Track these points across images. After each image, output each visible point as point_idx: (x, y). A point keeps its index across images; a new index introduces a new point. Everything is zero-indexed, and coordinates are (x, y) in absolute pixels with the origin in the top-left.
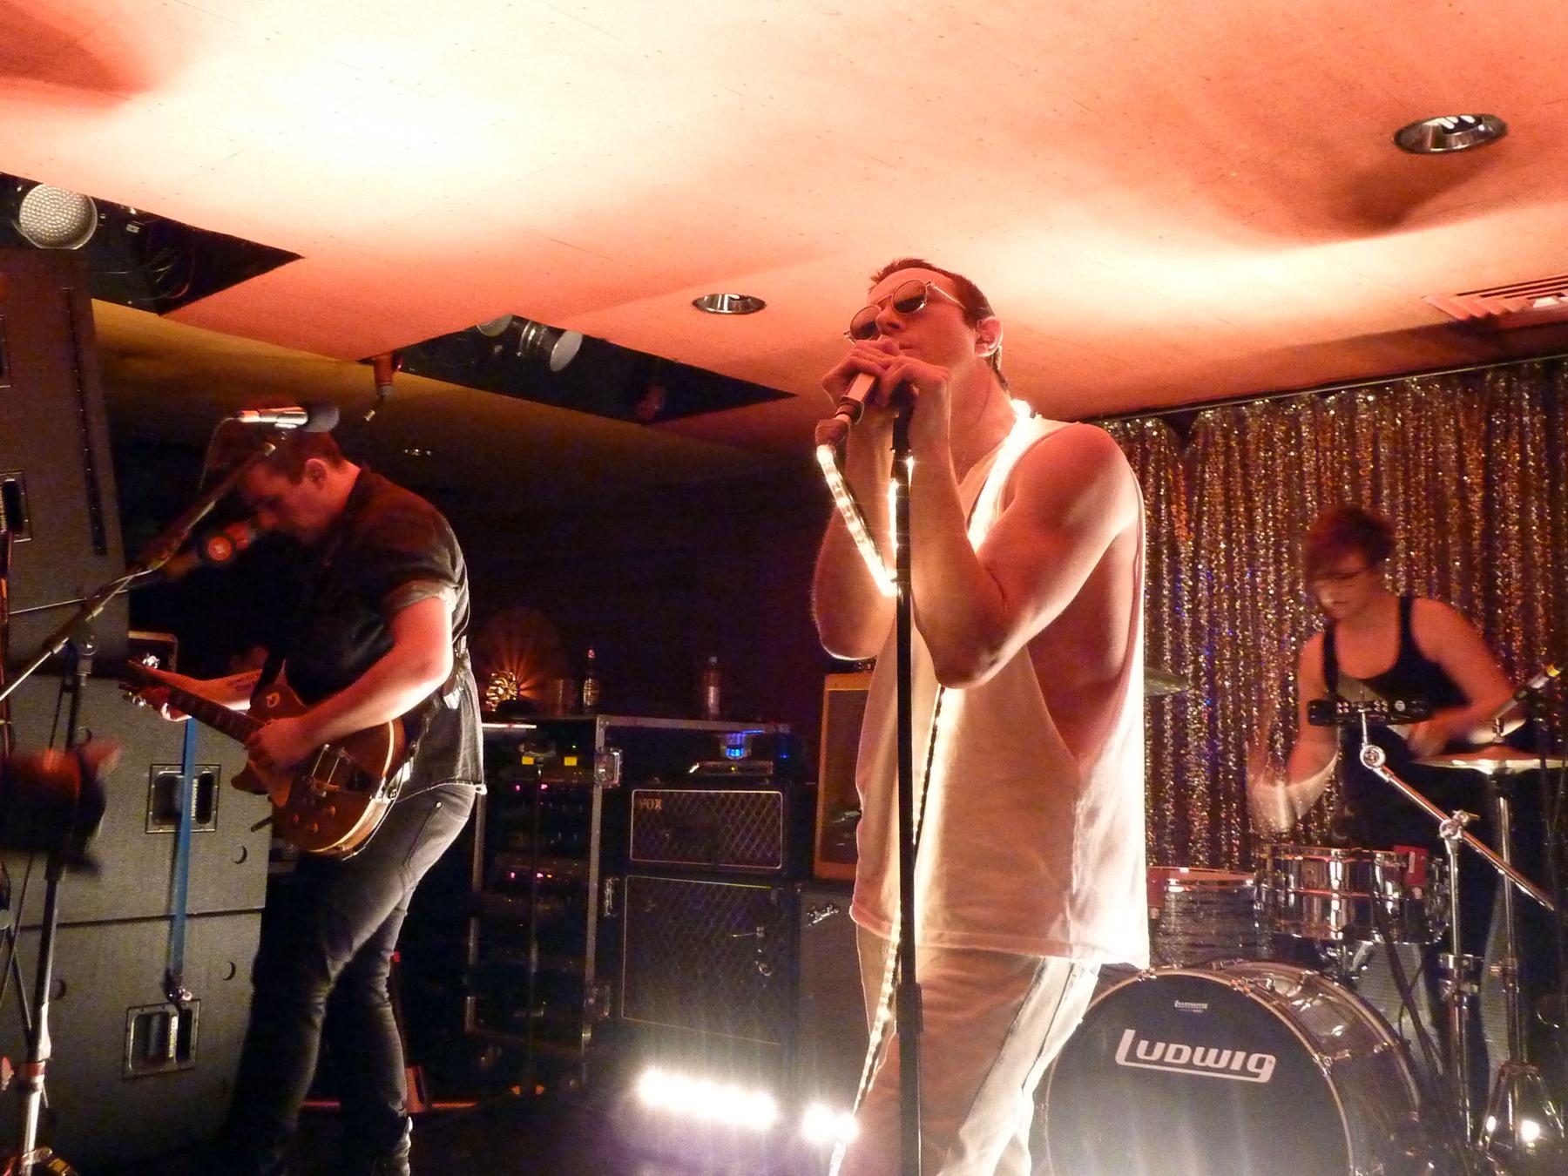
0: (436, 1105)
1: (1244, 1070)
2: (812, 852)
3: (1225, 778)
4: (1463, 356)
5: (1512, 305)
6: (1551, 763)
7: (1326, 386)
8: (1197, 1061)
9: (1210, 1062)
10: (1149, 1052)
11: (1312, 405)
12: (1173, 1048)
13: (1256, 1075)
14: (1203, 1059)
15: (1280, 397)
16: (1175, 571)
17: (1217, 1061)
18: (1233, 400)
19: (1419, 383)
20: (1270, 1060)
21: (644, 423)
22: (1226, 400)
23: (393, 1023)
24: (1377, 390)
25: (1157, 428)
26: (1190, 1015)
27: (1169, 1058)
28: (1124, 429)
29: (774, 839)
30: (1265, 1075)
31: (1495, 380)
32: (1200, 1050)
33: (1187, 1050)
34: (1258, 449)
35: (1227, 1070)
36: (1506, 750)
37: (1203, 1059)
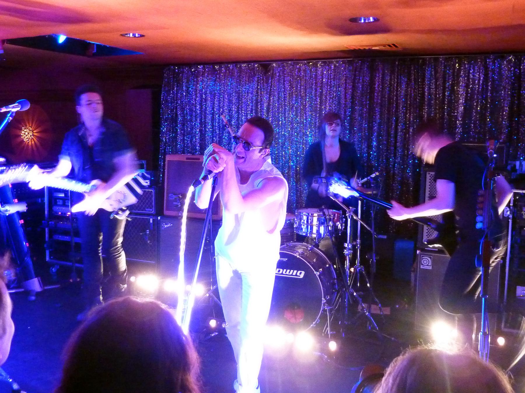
0: (46, 288)
1: (296, 275)
2: (163, 208)
4: (349, 56)
8: (284, 273)
9: (287, 273)
20: (303, 273)
21: (89, 56)
28: (248, 66)
29: (151, 203)
30: (302, 276)
32: (285, 270)
33: (281, 270)
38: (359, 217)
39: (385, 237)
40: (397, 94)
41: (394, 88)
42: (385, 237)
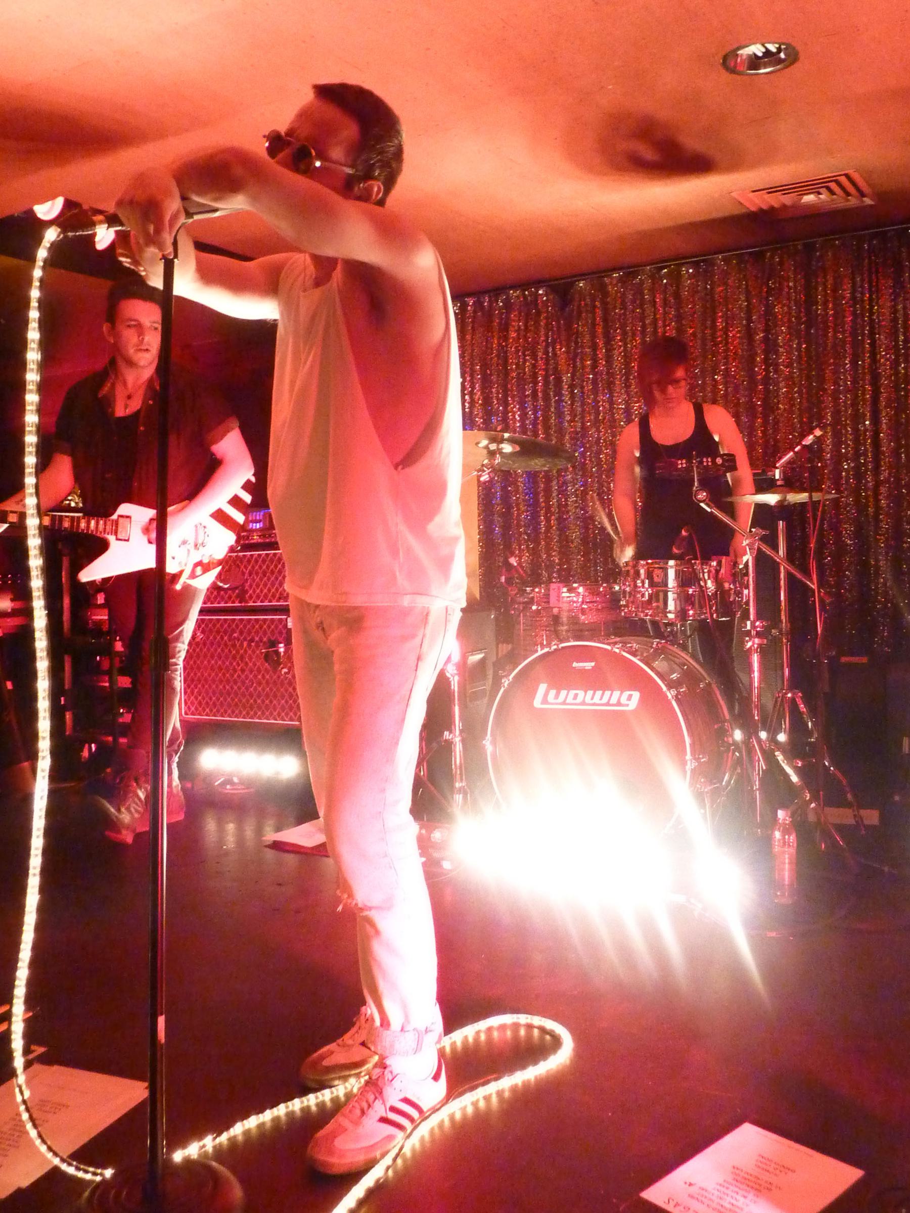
1: (619, 704)
3: (593, 532)
5: (787, 200)
6: (817, 496)
7: (660, 263)
9: (596, 700)
10: (557, 696)
11: (652, 277)
12: (572, 692)
13: (627, 705)
14: (592, 699)
15: (630, 271)
16: (558, 393)
17: (601, 699)
18: (597, 274)
19: (724, 260)
20: (636, 695)
22: (594, 273)
23: (252, 1122)
24: (696, 265)
25: (546, 295)
26: (583, 671)
27: (570, 700)
28: (525, 296)
31: (772, 257)
33: (581, 693)
34: (615, 308)
35: (608, 704)
36: (784, 489)
37: (592, 699)
38: (782, 552)
39: (865, 660)
40: (872, 321)
41: (863, 308)
42: (865, 660)
